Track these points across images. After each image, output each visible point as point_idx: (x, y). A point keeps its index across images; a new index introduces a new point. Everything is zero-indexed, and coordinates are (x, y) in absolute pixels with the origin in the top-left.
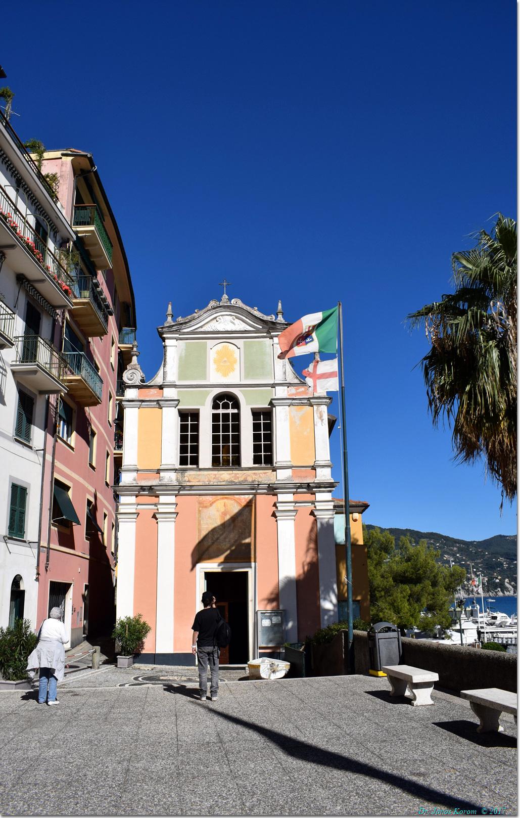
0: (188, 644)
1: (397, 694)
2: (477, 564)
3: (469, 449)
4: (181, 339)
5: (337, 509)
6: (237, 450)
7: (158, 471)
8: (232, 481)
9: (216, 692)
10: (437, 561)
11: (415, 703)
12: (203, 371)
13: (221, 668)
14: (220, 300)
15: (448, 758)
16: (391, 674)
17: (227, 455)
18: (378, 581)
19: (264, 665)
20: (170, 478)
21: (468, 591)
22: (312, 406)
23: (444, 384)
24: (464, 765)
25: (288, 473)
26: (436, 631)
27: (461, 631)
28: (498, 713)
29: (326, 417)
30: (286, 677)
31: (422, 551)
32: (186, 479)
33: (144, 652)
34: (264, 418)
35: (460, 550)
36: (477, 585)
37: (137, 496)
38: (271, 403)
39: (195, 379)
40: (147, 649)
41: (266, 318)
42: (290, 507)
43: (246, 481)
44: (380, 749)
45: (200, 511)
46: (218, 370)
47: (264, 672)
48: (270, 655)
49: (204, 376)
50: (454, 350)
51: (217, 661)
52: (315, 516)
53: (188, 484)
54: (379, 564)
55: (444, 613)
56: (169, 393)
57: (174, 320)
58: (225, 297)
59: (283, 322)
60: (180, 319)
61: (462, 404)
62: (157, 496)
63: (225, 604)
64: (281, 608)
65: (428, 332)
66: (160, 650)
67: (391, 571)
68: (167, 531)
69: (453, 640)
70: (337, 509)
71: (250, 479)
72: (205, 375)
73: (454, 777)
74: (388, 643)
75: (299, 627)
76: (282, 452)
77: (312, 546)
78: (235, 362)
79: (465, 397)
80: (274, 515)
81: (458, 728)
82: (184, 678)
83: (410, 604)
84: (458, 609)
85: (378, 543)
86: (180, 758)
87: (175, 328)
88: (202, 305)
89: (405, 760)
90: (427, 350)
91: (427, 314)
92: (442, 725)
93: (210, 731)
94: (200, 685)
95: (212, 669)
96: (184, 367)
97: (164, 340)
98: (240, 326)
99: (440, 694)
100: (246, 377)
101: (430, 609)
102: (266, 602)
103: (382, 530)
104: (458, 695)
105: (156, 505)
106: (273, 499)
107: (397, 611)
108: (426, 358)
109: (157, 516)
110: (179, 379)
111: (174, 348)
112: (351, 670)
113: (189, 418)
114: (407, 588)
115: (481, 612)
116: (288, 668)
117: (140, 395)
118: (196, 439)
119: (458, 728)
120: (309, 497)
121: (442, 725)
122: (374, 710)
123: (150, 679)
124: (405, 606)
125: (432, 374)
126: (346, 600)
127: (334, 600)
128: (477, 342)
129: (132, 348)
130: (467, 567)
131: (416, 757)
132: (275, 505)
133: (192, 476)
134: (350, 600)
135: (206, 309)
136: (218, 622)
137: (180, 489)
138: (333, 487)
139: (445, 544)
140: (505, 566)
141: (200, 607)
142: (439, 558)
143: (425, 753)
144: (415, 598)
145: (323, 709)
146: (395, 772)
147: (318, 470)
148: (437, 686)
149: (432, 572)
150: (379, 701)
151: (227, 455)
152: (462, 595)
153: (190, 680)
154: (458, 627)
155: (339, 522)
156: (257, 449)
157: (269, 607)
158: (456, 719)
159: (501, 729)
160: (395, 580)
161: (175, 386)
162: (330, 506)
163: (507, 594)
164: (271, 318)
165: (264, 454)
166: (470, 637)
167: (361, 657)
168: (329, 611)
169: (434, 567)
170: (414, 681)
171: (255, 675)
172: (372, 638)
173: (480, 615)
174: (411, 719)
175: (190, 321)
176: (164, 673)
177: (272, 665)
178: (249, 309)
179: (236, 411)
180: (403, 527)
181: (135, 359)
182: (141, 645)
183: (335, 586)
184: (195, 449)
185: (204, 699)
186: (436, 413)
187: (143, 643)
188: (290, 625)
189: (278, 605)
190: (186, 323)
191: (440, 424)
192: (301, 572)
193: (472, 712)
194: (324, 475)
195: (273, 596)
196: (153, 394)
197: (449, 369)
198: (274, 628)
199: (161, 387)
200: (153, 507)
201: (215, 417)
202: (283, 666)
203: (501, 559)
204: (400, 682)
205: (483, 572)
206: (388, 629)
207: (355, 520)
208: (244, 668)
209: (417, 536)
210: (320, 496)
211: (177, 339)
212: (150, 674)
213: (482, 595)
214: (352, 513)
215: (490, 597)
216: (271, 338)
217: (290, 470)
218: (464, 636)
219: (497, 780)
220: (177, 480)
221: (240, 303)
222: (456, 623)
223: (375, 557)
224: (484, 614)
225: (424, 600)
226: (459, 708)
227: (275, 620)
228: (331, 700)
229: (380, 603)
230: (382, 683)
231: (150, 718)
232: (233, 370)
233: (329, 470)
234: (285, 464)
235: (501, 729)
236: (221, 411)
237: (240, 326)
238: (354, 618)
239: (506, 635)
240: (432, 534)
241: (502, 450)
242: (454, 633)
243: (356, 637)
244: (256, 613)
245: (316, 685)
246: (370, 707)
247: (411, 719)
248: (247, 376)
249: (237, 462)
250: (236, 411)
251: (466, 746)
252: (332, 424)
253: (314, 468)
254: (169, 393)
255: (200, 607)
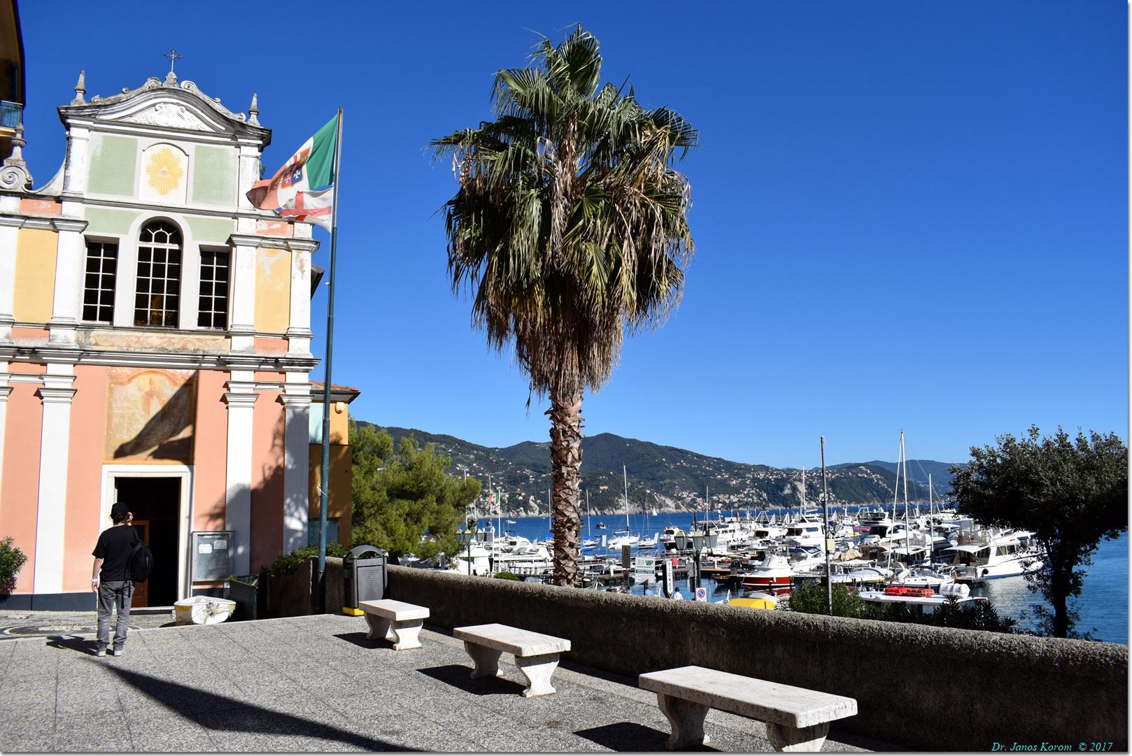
0: (84, 575)
1: (377, 637)
2: (497, 476)
3: (498, 329)
4: (96, 130)
5: (316, 396)
6: (174, 303)
7: (48, 327)
8: (164, 349)
9: (122, 643)
10: (446, 471)
11: (397, 646)
12: (129, 184)
13: (132, 613)
14: (163, 80)
15: (431, 712)
16: (371, 612)
17: (157, 308)
18: (367, 495)
19: (198, 607)
20: (67, 338)
21: (483, 511)
22: (289, 250)
23: (469, 239)
24: (451, 717)
25: (249, 341)
26: (439, 560)
27: (470, 560)
28: (703, 711)
29: (308, 268)
30: (229, 620)
31: (427, 457)
32: (92, 340)
33: (14, 593)
34: (218, 262)
35: (478, 458)
36: (494, 502)
37: (10, 362)
38: (230, 241)
39: (115, 193)
40: (21, 587)
41: (232, 116)
42: (249, 389)
43: (184, 349)
44: (345, 705)
45: (111, 389)
46: (152, 183)
47: (198, 615)
48: (209, 593)
49: (130, 191)
50: (487, 194)
51: (128, 602)
52: (283, 404)
53: (95, 348)
54: (370, 472)
55: (450, 537)
56: (70, 210)
57: (87, 99)
58: (172, 75)
59: (258, 125)
60: (97, 99)
61: (490, 268)
62: (44, 364)
63: (146, 523)
64: (228, 528)
65: (456, 169)
66: (41, 589)
67: (385, 483)
68: (57, 418)
69: (460, 570)
70: (316, 396)
71: (191, 347)
72: (132, 188)
73: (435, 733)
74: (369, 573)
75: (253, 555)
76: (241, 311)
77: (278, 442)
78: (180, 174)
79: (496, 259)
80: (224, 399)
81: (449, 675)
82: (78, 628)
83: (407, 525)
84: (468, 532)
85: (368, 445)
86: (58, 735)
87: (87, 112)
88: (135, 83)
89: (376, 717)
90: (453, 194)
91: (456, 142)
92: (429, 672)
93: (106, 696)
94: (98, 636)
95: (119, 612)
96: (98, 174)
97: (68, 127)
98: (190, 121)
99: (431, 634)
100: (195, 199)
101: (433, 531)
102: (207, 519)
103: (378, 428)
104: (633, 681)
105: (41, 377)
106: (224, 377)
107: (390, 532)
108: (449, 203)
109: (43, 393)
110: (90, 190)
111: (84, 142)
112: (319, 607)
113: (101, 253)
114: (406, 505)
115: (496, 536)
116: (232, 609)
117: (22, 207)
118: (110, 282)
119: (449, 675)
120: (276, 377)
121: (429, 672)
122: (344, 658)
123: (23, 631)
124: (401, 528)
125: (455, 224)
126: (319, 519)
127: (305, 518)
128: (513, 187)
129: (14, 134)
130: (485, 480)
131: (390, 711)
132: (226, 386)
133: (101, 337)
134: (324, 517)
135: (140, 90)
136: (133, 545)
137: (82, 355)
138: (312, 365)
139: (459, 450)
140: (532, 479)
141: (106, 523)
142: (451, 468)
143: (402, 707)
144: (413, 518)
145: (275, 659)
146: (362, 732)
147: (292, 340)
148: (427, 624)
149: (438, 485)
150: (351, 645)
151: (157, 308)
152: (476, 515)
153: (86, 630)
154: (465, 554)
155: (316, 412)
156: (204, 304)
157: (211, 527)
158: (447, 663)
159: (500, 673)
160: (390, 493)
161: (82, 200)
162: (306, 390)
163: (531, 514)
164: (241, 117)
165: (215, 313)
166: (481, 566)
167: (334, 591)
168: (296, 531)
169: (442, 479)
170: (398, 618)
171: (185, 619)
172: (348, 566)
173: (495, 540)
174: (390, 666)
175: (113, 104)
176: (45, 622)
177: (209, 605)
178: (207, 98)
179: (176, 247)
180: (434, 431)
181: (17, 151)
182: (12, 583)
183: (307, 501)
184: (109, 298)
185: (103, 653)
186: (457, 277)
187: (13, 580)
188: (240, 550)
189: (224, 525)
190: (106, 106)
191: (461, 292)
192: (260, 478)
193: (467, 655)
194: (300, 348)
195: (217, 511)
196: (44, 208)
197: (478, 221)
198: (218, 554)
199: (59, 200)
200: (36, 379)
201: (144, 253)
202: (226, 607)
203: (527, 472)
204: (379, 621)
205: (503, 487)
206: (370, 555)
207: (339, 412)
208: (170, 612)
209: (423, 438)
210: (292, 377)
211: (90, 129)
212: (24, 624)
213: (500, 514)
214: (335, 402)
215: (510, 518)
216: (238, 146)
217: (251, 338)
218: (475, 563)
219: (487, 733)
220: (78, 341)
221: (194, 89)
222: (463, 549)
223: (365, 462)
224: (500, 539)
225: (425, 520)
226: (452, 650)
227: (220, 544)
228: (287, 648)
229: (368, 524)
230: (358, 624)
231: (14, 684)
232: (176, 186)
233: (308, 341)
234: (244, 329)
235: (500, 673)
236: (153, 245)
237: (190, 121)
238: (329, 539)
239: (525, 565)
240: (444, 436)
241: (532, 332)
242: (461, 562)
243: (329, 566)
244: (190, 535)
245: (268, 629)
246: (339, 654)
247: (390, 666)
248: (196, 197)
249: (173, 321)
250: (176, 247)
251: (456, 695)
252: (316, 279)
253: (286, 337)
254: (70, 210)
255: (106, 523)
